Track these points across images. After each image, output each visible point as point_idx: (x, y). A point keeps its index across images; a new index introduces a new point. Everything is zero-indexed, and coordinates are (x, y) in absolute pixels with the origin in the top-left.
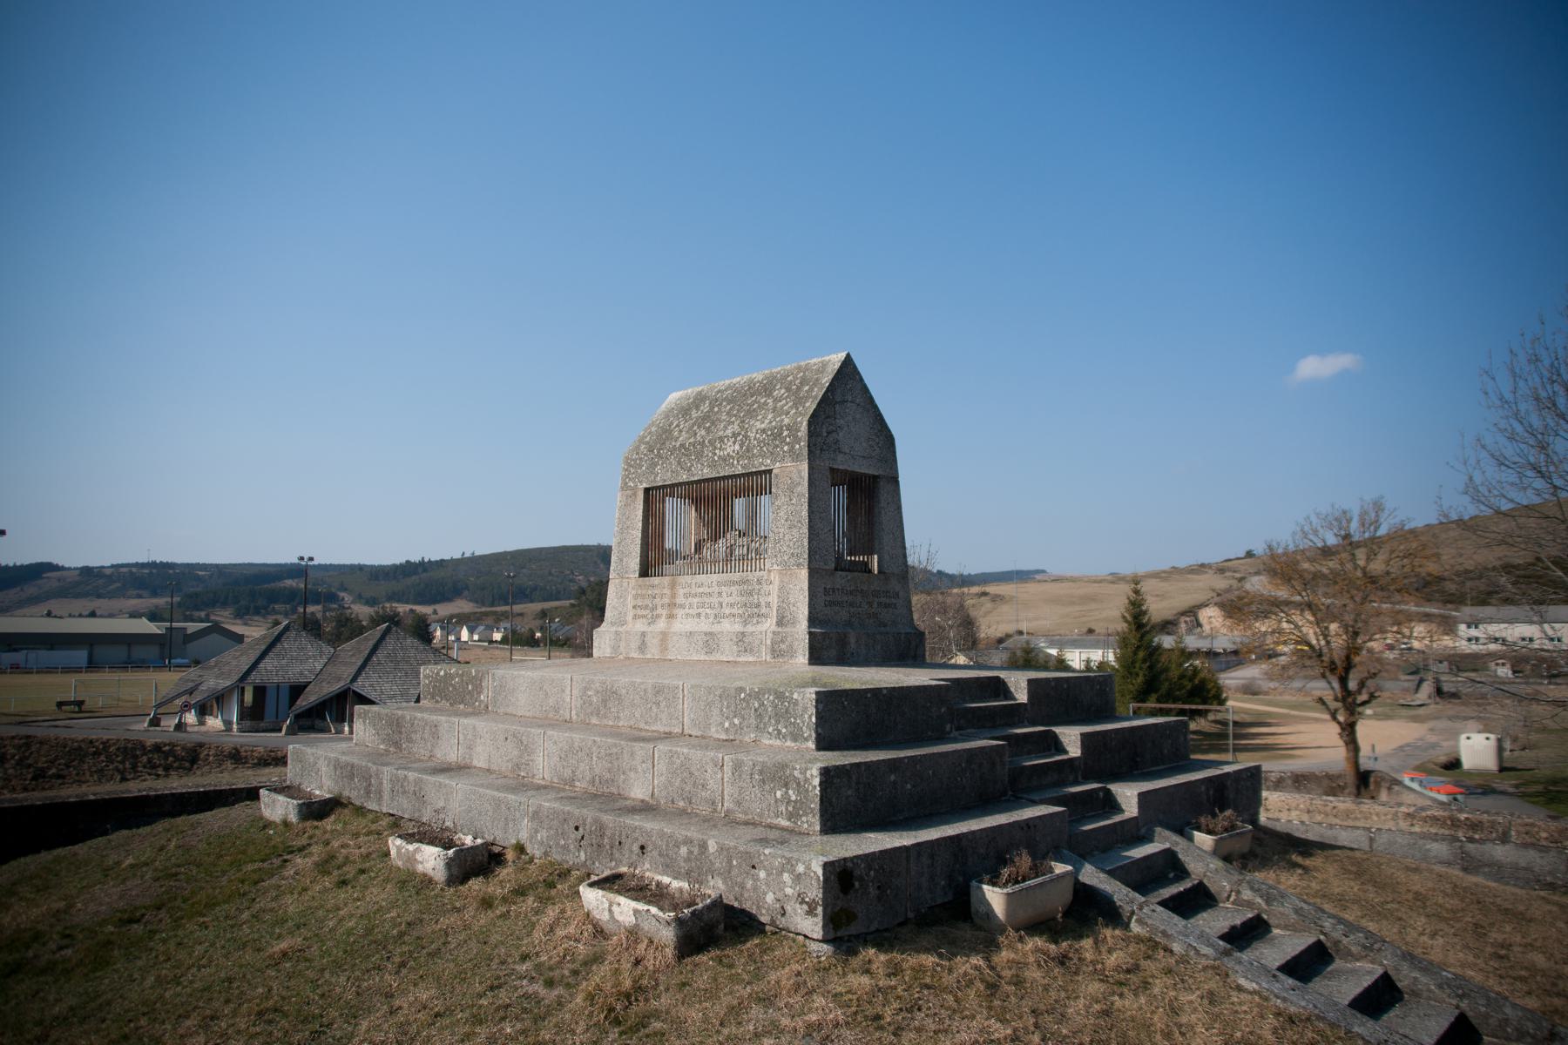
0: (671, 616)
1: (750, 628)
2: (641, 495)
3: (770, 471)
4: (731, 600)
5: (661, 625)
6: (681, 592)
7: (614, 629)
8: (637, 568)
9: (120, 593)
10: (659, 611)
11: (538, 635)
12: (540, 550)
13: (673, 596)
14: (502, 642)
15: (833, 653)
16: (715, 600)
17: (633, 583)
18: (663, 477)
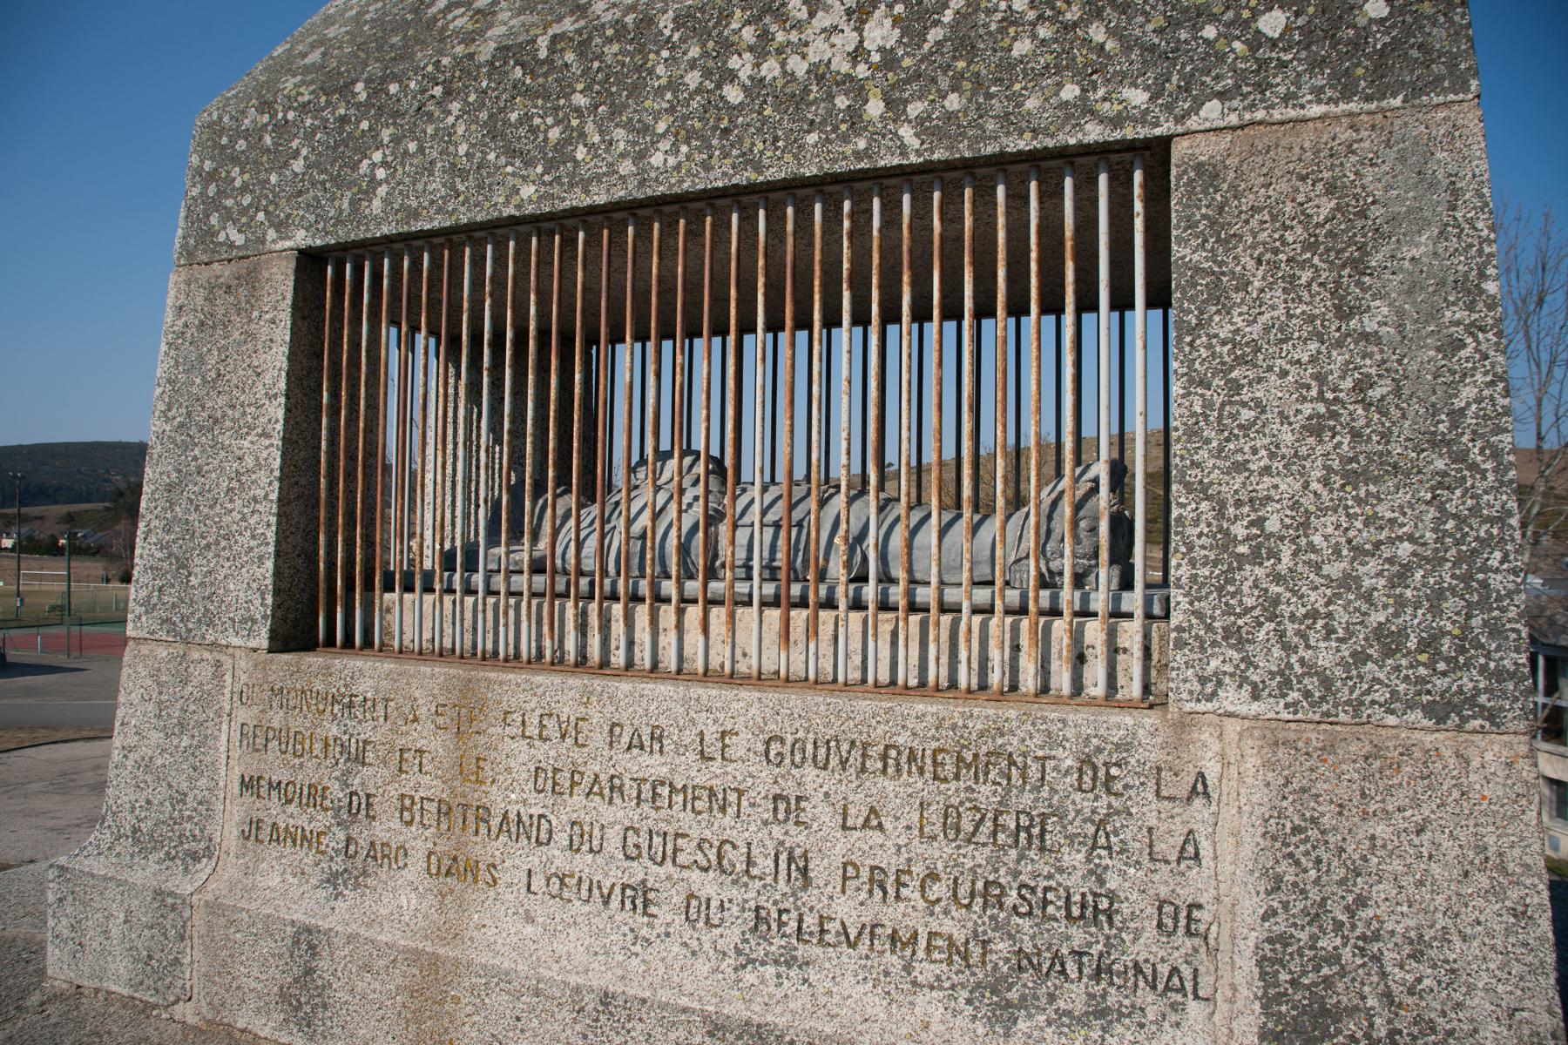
0: (456, 869)
2: (281, 283)
3: (1156, 153)
4: (880, 849)
5: (401, 904)
6: (519, 757)
7: (146, 873)
8: (262, 606)
9: (377, 407)
10: (386, 828)
11: (63, 541)
12: (67, 446)
13: (471, 769)
14: (12, 550)
16: (752, 832)
18: (395, 193)
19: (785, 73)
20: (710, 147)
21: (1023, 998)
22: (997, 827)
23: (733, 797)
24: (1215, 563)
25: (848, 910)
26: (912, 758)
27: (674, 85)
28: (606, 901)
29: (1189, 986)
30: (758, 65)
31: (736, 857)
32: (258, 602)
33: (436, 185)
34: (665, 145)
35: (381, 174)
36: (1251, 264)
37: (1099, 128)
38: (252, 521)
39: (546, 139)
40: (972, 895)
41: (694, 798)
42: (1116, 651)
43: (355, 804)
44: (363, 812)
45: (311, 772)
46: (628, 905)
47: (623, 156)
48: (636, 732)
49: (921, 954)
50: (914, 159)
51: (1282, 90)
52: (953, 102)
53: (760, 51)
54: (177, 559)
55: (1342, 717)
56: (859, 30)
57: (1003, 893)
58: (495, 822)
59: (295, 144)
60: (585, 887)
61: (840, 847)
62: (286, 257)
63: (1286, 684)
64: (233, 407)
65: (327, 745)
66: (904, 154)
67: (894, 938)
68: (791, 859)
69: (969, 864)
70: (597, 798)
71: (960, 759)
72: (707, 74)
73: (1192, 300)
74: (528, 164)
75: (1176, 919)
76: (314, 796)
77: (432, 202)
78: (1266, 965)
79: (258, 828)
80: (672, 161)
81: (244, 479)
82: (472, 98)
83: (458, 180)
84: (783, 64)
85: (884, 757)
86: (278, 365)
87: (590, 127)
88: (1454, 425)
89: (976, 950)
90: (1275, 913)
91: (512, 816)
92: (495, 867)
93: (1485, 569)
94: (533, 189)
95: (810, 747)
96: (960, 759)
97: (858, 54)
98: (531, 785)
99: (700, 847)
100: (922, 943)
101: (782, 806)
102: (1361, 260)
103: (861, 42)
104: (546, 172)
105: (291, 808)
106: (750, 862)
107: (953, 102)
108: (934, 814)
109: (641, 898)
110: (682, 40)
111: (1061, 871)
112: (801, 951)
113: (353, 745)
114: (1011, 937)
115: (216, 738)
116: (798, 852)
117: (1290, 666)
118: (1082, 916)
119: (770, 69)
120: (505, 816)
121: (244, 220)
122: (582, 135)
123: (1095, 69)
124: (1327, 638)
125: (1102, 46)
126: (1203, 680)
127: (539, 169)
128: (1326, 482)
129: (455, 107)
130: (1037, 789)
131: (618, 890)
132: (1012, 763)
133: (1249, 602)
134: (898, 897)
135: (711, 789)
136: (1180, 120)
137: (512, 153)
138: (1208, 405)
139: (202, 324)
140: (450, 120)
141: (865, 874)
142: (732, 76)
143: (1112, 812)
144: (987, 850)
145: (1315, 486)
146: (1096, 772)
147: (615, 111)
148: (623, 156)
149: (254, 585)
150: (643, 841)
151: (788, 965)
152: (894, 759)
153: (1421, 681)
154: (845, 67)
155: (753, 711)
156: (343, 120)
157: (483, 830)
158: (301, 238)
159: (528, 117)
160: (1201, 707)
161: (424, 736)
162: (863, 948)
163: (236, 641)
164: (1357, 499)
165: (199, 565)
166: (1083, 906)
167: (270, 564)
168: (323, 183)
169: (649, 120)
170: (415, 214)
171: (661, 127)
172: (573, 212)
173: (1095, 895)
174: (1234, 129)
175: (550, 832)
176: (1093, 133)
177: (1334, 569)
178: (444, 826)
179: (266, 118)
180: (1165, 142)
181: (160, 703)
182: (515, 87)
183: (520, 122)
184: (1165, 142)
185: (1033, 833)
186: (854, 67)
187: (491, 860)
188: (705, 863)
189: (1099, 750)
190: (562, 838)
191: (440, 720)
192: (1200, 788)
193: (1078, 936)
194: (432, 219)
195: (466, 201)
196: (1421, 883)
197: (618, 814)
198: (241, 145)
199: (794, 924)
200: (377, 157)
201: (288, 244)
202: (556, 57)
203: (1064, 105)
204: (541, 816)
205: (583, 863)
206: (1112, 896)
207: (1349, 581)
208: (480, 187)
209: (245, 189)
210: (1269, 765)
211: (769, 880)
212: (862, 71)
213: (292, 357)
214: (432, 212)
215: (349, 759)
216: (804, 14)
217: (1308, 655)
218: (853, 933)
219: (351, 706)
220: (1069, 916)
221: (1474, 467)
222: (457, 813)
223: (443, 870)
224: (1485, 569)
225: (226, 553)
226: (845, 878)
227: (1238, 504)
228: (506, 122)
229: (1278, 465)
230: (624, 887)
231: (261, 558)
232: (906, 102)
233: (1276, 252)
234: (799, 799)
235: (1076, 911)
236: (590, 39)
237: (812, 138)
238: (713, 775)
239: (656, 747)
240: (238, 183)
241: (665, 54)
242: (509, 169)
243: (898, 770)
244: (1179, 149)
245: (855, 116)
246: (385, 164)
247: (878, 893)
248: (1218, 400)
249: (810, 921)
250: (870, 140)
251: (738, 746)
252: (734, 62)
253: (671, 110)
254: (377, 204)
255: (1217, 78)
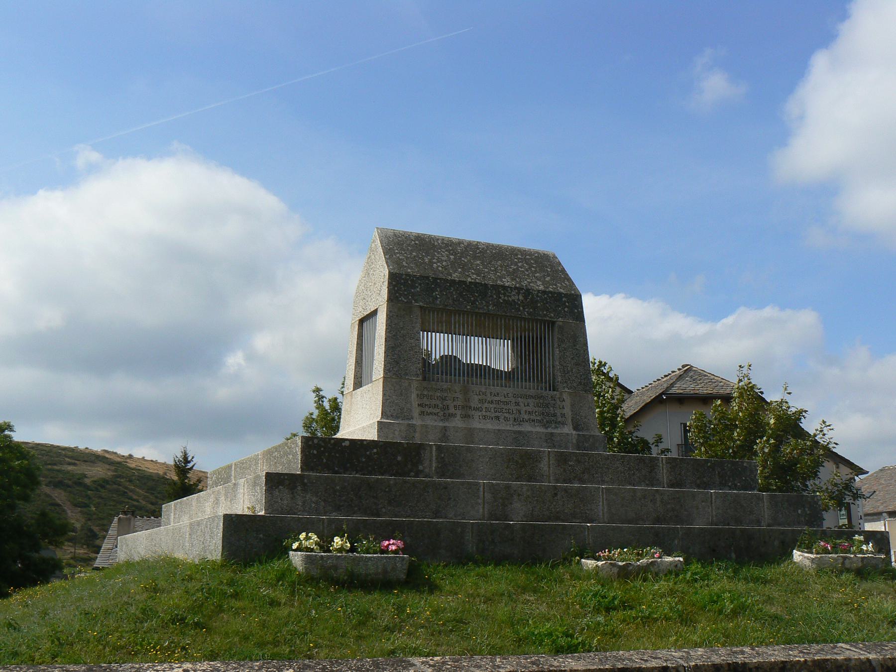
4: (529, 409)
13: (467, 400)
16: (513, 407)
25: (526, 417)
42: (227, 480)
45: (434, 402)
61: (524, 409)
109: (498, 418)
161: (458, 395)
185: (547, 406)
251: (510, 395)
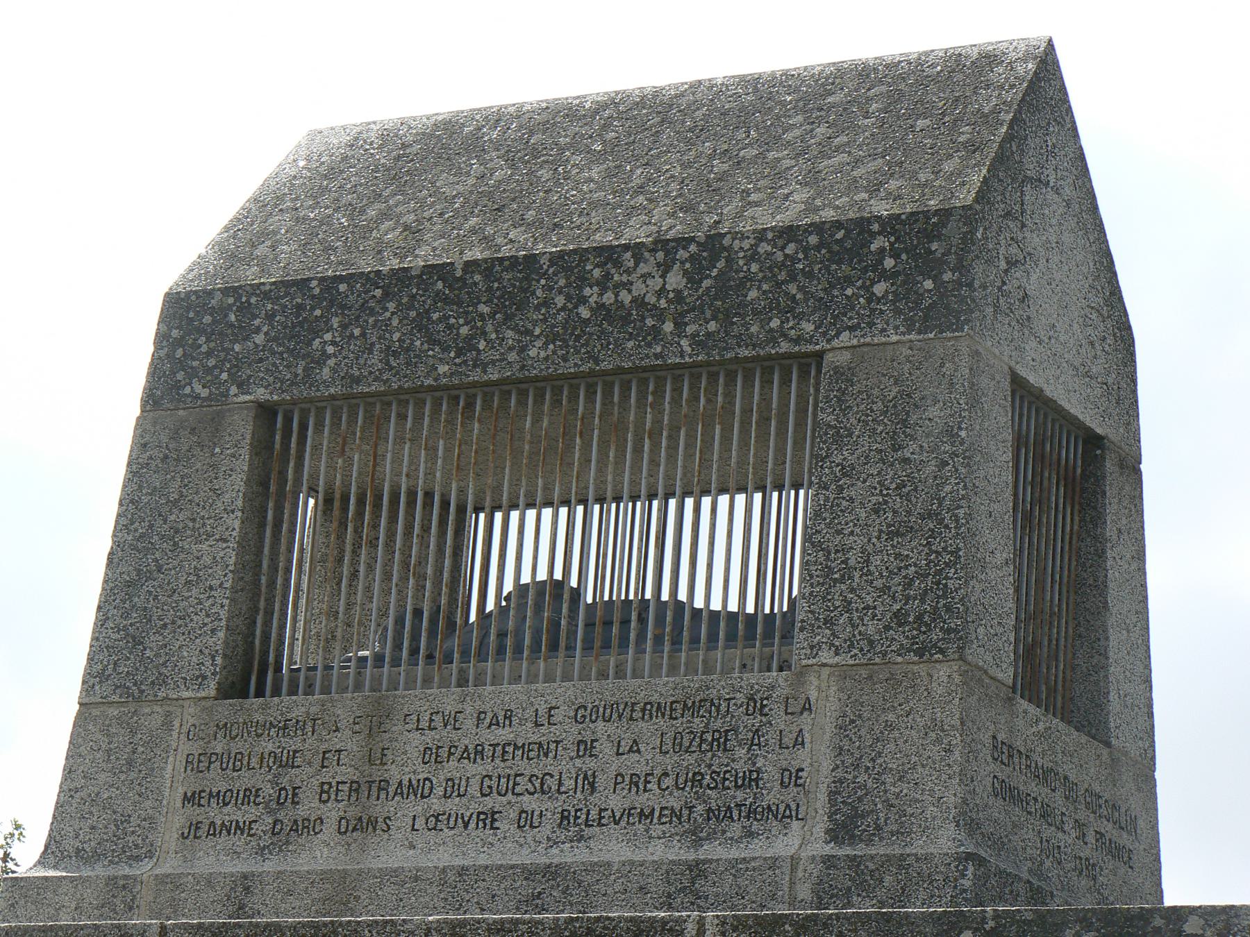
1: (714, 851)
2: (242, 428)
4: (636, 764)
10: (309, 806)
15: (1134, 566)
16: (565, 766)
17: (189, 716)
19: (617, 301)
20: (567, 346)
21: (709, 834)
22: (702, 741)
23: (553, 746)
24: (823, 584)
26: (659, 708)
27: (546, 303)
28: (466, 825)
29: (794, 813)
30: (601, 295)
31: (552, 783)
32: (208, 664)
33: (375, 360)
34: (539, 343)
35: (330, 350)
36: (855, 422)
37: (787, 345)
38: (207, 605)
39: (458, 334)
40: (686, 782)
41: (529, 751)
43: (283, 796)
44: (289, 801)
45: (246, 780)
46: (481, 824)
47: (511, 349)
48: (495, 716)
49: (655, 821)
50: (687, 359)
51: (880, 326)
52: (712, 326)
53: (603, 284)
54: (134, 638)
55: (877, 660)
56: (663, 276)
57: (703, 778)
58: (392, 790)
59: (257, 322)
60: (452, 819)
62: (247, 408)
63: (852, 646)
64: (194, 520)
65: (262, 758)
66: (682, 356)
67: (641, 814)
68: (586, 777)
69: (685, 764)
70: (466, 761)
71: (685, 705)
72: (569, 298)
73: (824, 443)
74: (445, 349)
75: (790, 778)
76: (250, 796)
77: (371, 373)
78: (832, 794)
79: (197, 828)
80: (543, 354)
81: (201, 573)
82: (405, 300)
83: (392, 359)
84: (617, 295)
85: (644, 710)
86: (237, 487)
87: (489, 328)
88: (940, 505)
89: (685, 812)
90: (838, 767)
91: (405, 782)
92: (389, 818)
93: (947, 578)
94: (447, 367)
95: (601, 710)
96: (685, 705)
97: (661, 292)
98: (420, 760)
99: (530, 780)
100: (657, 814)
101: (582, 748)
102: (906, 420)
103: (664, 285)
104: (457, 356)
105: (226, 810)
106: (560, 784)
107: (712, 326)
108: (668, 740)
110: (555, 274)
111: (733, 761)
112: (587, 832)
113: (285, 754)
114: (705, 802)
115: (163, 769)
116: (590, 773)
117: (854, 636)
118: (743, 784)
119: (608, 298)
120: (400, 784)
121: (209, 378)
122: (484, 333)
123: (790, 310)
124: (873, 619)
125: (794, 296)
126: (812, 647)
127: (452, 354)
128: (879, 538)
129: (391, 306)
130: (724, 717)
131: (475, 816)
132: (712, 704)
133: (837, 603)
134: (645, 791)
135: (540, 744)
136: (828, 341)
137: (433, 342)
138: (827, 499)
139: (166, 457)
140: (388, 314)
141: (627, 779)
142: (583, 300)
143: (762, 724)
144: (695, 755)
145: (874, 540)
146: (756, 704)
147: (508, 318)
148: (511, 349)
149: (207, 651)
150: (494, 783)
151: (579, 841)
152: (651, 710)
153: (914, 637)
154: (653, 300)
155: (569, 692)
156: (300, 307)
157: (383, 795)
158: (261, 394)
159: (446, 318)
160: (810, 662)
162: (623, 824)
163: (186, 694)
164: (893, 546)
165: (153, 641)
166: (744, 780)
167: (221, 634)
168: (281, 354)
169: (530, 326)
170: (357, 381)
171: (537, 331)
172: (474, 385)
173: (751, 772)
174: (854, 347)
175: (431, 789)
176: (784, 347)
177: (879, 583)
178: (353, 799)
179: (231, 301)
180: (820, 355)
181: (108, 751)
182: (437, 295)
183: (440, 320)
184: (820, 355)
185: (721, 742)
186: (658, 300)
187: (387, 814)
188: (532, 790)
189: (758, 691)
190: (439, 791)
191: (357, 727)
192: (807, 707)
193: (740, 795)
194: (370, 385)
195: (397, 373)
196: (907, 741)
197: (475, 769)
198: (207, 319)
199: (584, 817)
200: (328, 337)
201: (248, 398)
202: (468, 276)
203: (771, 330)
204: (425, 779)
205: (453, 805)
206: (758, 771)
207: (885, 589)
208: (408, 364)
209: (209, 354)
210: (841, 690)
211: (571, 793)
212: (663, 303)
213: (248, 482)
214: (370, 380)
215: (280, 766)
216: (631, 264)
217: (862, 629)
218: (618, 815)
219: (285, 727)
220: (737, 787)
221: (947, 527)
222: (364, 788)
223: (350, 828)
224: (947, 578)
225: (182, 630)
226: (616, 784)
227: (837, 551)
228: (429, 319)
229: (857, 530)
230: (479, 814)
231: (213, 631)
232: (686, 324)
233: (867, 415)
234: (593, 741)
235: (740, 782)
236: (494, 266)
237: (630, 344)
238: (545, 734)
239: (507, 722)
240: (204, 349)
241: (543, 282)
242: (431, 353)
243: (651, 718)
244: (829, 357)
245: (656, 332)
246: (333, 343)
247: (634, 789)
248: (832, 497)
249: (594, 814)
250: (663, 346)
251: (558, 715)
252: (587, 291)
253: (545, 320)
254: (326, 371)
255: (851, 318)
